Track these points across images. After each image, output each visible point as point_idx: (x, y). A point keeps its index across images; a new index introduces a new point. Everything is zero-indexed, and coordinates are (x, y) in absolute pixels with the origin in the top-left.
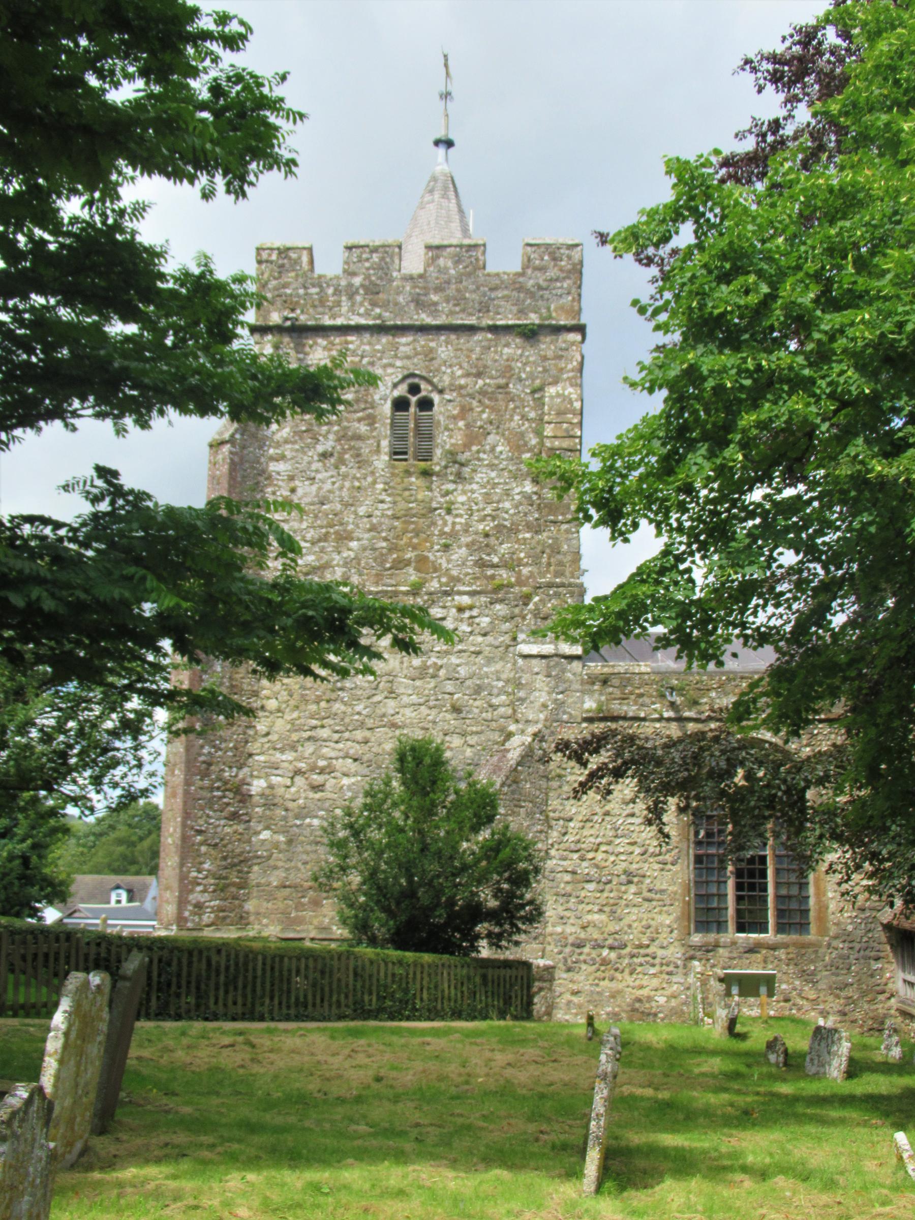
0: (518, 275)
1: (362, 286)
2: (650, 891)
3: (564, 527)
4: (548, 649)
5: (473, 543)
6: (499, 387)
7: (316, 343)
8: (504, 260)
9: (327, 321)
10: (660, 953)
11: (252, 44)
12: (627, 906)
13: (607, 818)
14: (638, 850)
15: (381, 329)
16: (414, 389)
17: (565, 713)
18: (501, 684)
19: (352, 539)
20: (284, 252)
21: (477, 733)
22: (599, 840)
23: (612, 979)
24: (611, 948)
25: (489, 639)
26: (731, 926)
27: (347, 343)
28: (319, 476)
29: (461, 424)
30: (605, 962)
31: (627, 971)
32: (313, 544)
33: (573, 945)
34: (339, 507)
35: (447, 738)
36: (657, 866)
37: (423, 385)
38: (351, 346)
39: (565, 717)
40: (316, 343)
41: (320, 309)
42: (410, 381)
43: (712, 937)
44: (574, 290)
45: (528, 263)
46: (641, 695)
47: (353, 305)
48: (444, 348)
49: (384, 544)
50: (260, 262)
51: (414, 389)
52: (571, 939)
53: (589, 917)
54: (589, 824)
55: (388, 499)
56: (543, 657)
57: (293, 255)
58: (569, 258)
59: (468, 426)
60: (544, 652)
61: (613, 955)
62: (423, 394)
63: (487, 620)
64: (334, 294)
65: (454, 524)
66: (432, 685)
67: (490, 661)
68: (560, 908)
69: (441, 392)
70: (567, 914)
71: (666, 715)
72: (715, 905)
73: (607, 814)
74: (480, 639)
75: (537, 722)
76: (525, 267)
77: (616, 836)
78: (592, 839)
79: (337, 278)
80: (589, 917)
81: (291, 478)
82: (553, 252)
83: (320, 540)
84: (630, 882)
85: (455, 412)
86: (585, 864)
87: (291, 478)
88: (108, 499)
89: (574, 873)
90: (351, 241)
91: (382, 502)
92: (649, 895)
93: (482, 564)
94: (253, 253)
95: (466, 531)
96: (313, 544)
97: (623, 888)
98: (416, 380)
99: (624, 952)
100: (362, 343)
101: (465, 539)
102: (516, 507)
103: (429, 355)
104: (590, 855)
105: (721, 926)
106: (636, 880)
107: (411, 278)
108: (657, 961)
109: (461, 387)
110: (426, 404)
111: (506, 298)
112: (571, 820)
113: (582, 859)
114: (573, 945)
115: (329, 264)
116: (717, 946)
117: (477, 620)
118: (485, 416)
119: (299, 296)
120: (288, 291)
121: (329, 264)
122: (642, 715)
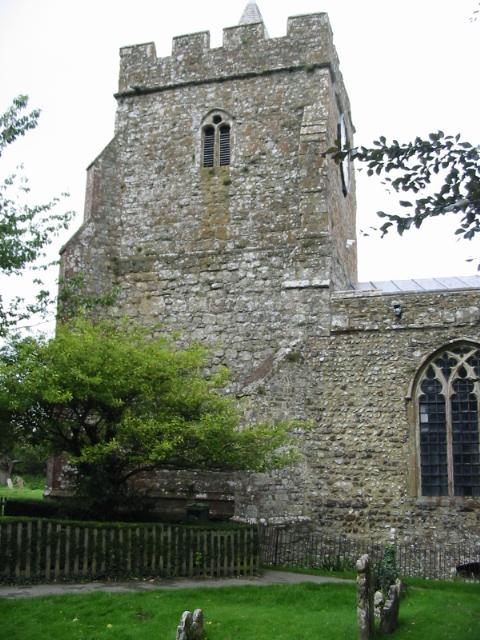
0: (284, 38)
1: (184, 60)
2: (385, 463)
3: (316, 195)
4: (304, 283)
5: (257, 216)
6: (274, 111)
7: (155, 100)
8: (276, 28)
9: (162, 85)
10: (394, 512)
11: (29, 103)
12: (367, 475)
13: (352, 408)
14: (375, 432)
15: (195, 84)
16: (217, 119)
17: (317, 329)
18: (277, 314)
19: (176, 221)
20: (135, 48)
21: (261, 350)
22: (345, 425)
23: (355, 531)
24: (355, 508)
25: (268, 282)
26: (451, 490)
27: (174, 96)
28: (156, 183)
29: (248, 138)
30: (351, 518)
31: (368, 525)
32: (151, 227)
33: (326, 506)
34: (167, 201)
35: (240, 354)
36: (390, 444)
37: (222, 115)
38: (177, 99)
39: (318, 333)
40: (155, 100)
41: (158, 79)
42: (213, 114)
43: (434, 499)
44: (322, 43)
45: (291, 29)
46: (375, 313)
47: (177, 73)
48: (236, 91)
49: (197, 223)
50: (122, 56)
51: (217, 119)
52: (324, 502)
53: (338, 484)
54: (337, 413)
55: (200, 192)
56: (300, 288)
57: (141, 49)
58: (319, 22)
59: (252, 139)
60: (302, 285)
61: (357, 513)
62: (223, 121)
63: (266, 268)
64: (166, 68)
65: (243, 206)
66: (229, 316)
67: (269, 297)
68: (316, 477)
69: (234, 118)
70: (322, 482)
71: (394, 327)
72: (437, 474)
73: (351, 404)
74: (262, 282)
75: (296, 338)
76: (289, 32)
77: (358, 421)
78: (340, 425)
79: (168, 58)
80: (338, 484)
81: (138, 186)
82: (305, 19)
83: (156, 224)
84: (369, 457)
85: (244, 131)
86: (334, 444)
87: (138, 186)
88: (417, 154)
89: (325, 450)
90: (175, 35)
91: (196, 195)
92: (384, 467)
93: (262, 230)
94: (119, 51)
95: (253, 208)
96: (151, 227)
97: (364, 461)
98: (218, 113)
99: (366, 511)
100: (184, 95)
101: (251, 214)
102: (287, 189)
103: (227, 97)
104: (338, 437)
105: (442, 491)
106: (374, 455)
107: (215, 50)
108: (391, 518)
109: (248, 114)
110: (225, 129)
111: (277, 54)
112: (324, 409)
113: (333, 439)
114: (326, 506)
115: (164, 50)
116: (438, 505)
117: (259, 269)
118: (264, 130)
119: (145, 72)
120: (138, 71)
121: (164, 50)
122: (376, 328)
